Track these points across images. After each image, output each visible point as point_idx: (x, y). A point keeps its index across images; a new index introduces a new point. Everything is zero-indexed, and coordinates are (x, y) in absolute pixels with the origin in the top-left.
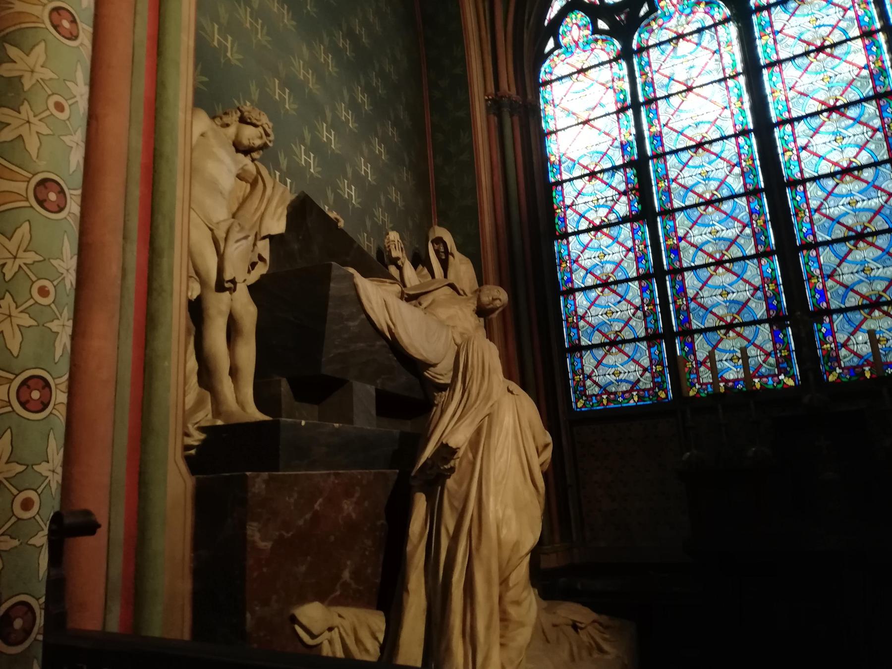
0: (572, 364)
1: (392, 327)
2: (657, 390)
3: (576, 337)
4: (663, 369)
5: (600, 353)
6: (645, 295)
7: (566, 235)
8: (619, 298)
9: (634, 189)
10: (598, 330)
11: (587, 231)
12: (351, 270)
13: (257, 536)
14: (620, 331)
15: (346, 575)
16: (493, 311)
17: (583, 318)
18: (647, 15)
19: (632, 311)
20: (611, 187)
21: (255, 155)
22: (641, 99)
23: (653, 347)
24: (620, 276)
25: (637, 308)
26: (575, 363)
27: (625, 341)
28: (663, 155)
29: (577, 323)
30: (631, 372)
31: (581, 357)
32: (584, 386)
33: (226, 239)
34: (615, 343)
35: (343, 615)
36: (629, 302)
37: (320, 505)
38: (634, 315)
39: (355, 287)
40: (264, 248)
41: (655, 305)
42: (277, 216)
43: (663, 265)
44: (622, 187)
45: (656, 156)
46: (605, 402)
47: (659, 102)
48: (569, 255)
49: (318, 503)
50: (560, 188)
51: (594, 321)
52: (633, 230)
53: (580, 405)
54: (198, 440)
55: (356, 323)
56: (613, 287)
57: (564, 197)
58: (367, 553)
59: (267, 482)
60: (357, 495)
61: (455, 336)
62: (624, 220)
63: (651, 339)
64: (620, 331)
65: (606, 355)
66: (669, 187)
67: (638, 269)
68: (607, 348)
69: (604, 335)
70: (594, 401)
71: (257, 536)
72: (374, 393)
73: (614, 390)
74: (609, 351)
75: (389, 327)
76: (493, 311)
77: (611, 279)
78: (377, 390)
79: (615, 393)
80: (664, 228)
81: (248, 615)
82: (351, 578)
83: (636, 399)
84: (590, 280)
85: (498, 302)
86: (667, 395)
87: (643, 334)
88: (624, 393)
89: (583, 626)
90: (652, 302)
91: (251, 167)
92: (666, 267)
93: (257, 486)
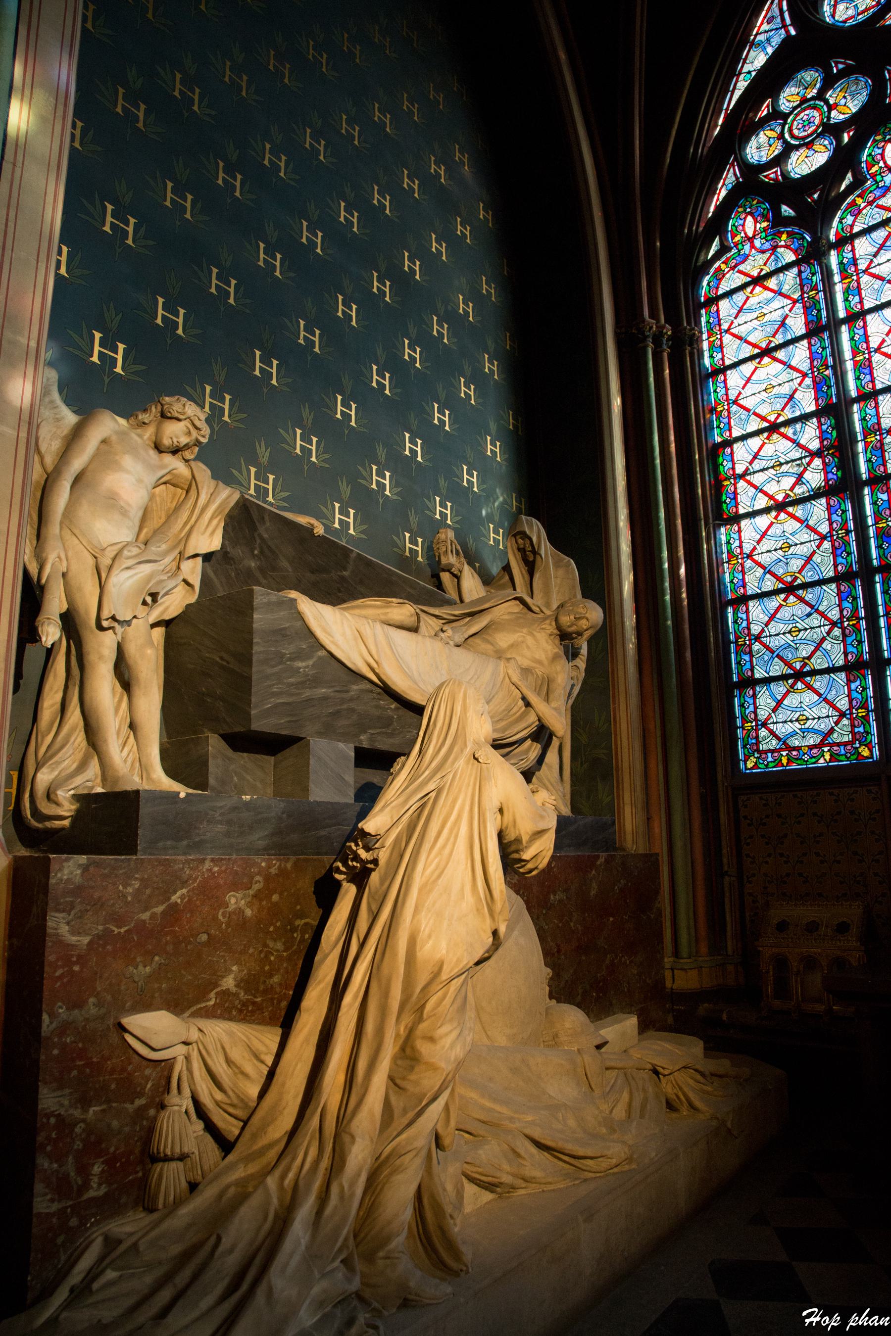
0: (742, 705)
1: (374, 665)
2: (858, 745)
3: (748, 666)
4: (868, 715)
5: (779, 689)
6: (845, 604)
7: (737, 519)
8: (808, 609)
9: (832, 447)
10: (778, 656)
11: (766, 511)
12: (293, 594)
13: (64, 929)
14: (809, 658)
15: (229, 983)
16: (580, 634)
17: (758, 638)
18: (850, 190)
19: (827, 628)
20: (799, 445)
21: (188, 455)
22: (842, 314)
23: (855, 681)
24: (809, 576)
25: (833, 624)
26: (746, 705)
27: (814, 673)
28: (875, 394)
29: (750, 646)
30: (820, 716)
31: (754, 696)
32: (757, 737)
33: (110, 568)
34: (799, 675)
35: (204, 1030)
36: (822, 615)
37: (182, 897)
38: (828, 633)
39: (300, 617)
40: (193, 570)
41: (859, 619)
42: (210, 529)
43: (871, 560)
44: (815, 445)
45: (863, 397)
46: (784, 761)
47: (869, 318)
48: (741, 547)
49: (179, 894)
50: (728, 450)
51: (773, 643)
52: (829, 507)
53: (750, 764)
54: (70, 810)
55: (311, 662)
56: (800, 592)
57: (734, 464)
58: (272, 958)
59: (85, 868)
60: (256, 887)
61: (510, 672)
62: (816, 495)
63: (852, 668)
64: (809, 658)
65: (788, 692)
66: (881, 441)
67: (835, 566)
68: (790, 681)
69: (787, 663)
70: (770, 759)
71: (64, 929)
72: (353, 754)
73: (797, 743)
74: (792, 686)
75: (369, 665)
76: (580, 634)
77: (799, 582)
78: (356, 748)
79: (798, 749)
80: (874, 503)
81: (45, 1017)
82: (237, 986)
83: (827, 757)
84: (769, 583)
85: (584, 622)
86: (871, 752)
87: (841, 662)
88: (811, 748)
89: (666, 1072)
90: (855, 615)
91: (182, 469)
92: (875, 563)
93: (66, 871)
